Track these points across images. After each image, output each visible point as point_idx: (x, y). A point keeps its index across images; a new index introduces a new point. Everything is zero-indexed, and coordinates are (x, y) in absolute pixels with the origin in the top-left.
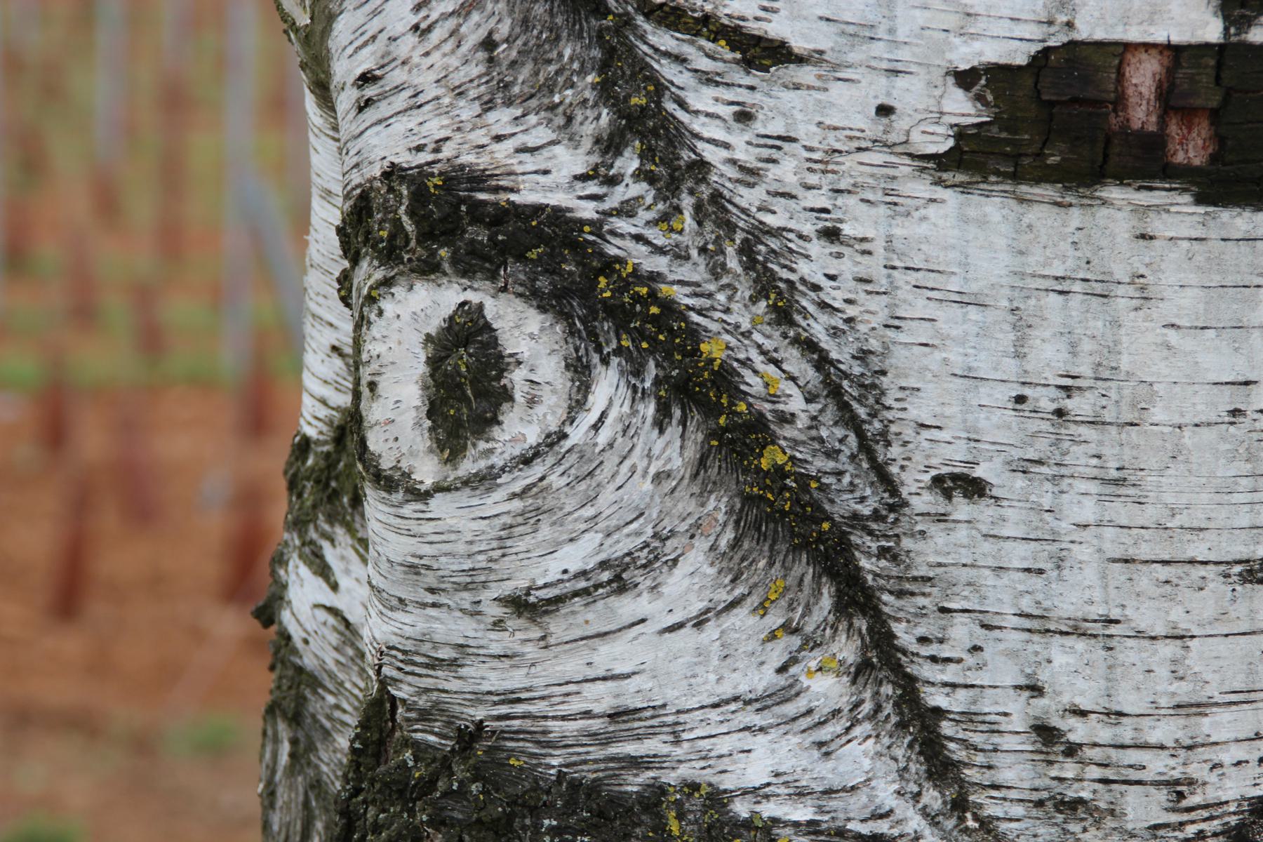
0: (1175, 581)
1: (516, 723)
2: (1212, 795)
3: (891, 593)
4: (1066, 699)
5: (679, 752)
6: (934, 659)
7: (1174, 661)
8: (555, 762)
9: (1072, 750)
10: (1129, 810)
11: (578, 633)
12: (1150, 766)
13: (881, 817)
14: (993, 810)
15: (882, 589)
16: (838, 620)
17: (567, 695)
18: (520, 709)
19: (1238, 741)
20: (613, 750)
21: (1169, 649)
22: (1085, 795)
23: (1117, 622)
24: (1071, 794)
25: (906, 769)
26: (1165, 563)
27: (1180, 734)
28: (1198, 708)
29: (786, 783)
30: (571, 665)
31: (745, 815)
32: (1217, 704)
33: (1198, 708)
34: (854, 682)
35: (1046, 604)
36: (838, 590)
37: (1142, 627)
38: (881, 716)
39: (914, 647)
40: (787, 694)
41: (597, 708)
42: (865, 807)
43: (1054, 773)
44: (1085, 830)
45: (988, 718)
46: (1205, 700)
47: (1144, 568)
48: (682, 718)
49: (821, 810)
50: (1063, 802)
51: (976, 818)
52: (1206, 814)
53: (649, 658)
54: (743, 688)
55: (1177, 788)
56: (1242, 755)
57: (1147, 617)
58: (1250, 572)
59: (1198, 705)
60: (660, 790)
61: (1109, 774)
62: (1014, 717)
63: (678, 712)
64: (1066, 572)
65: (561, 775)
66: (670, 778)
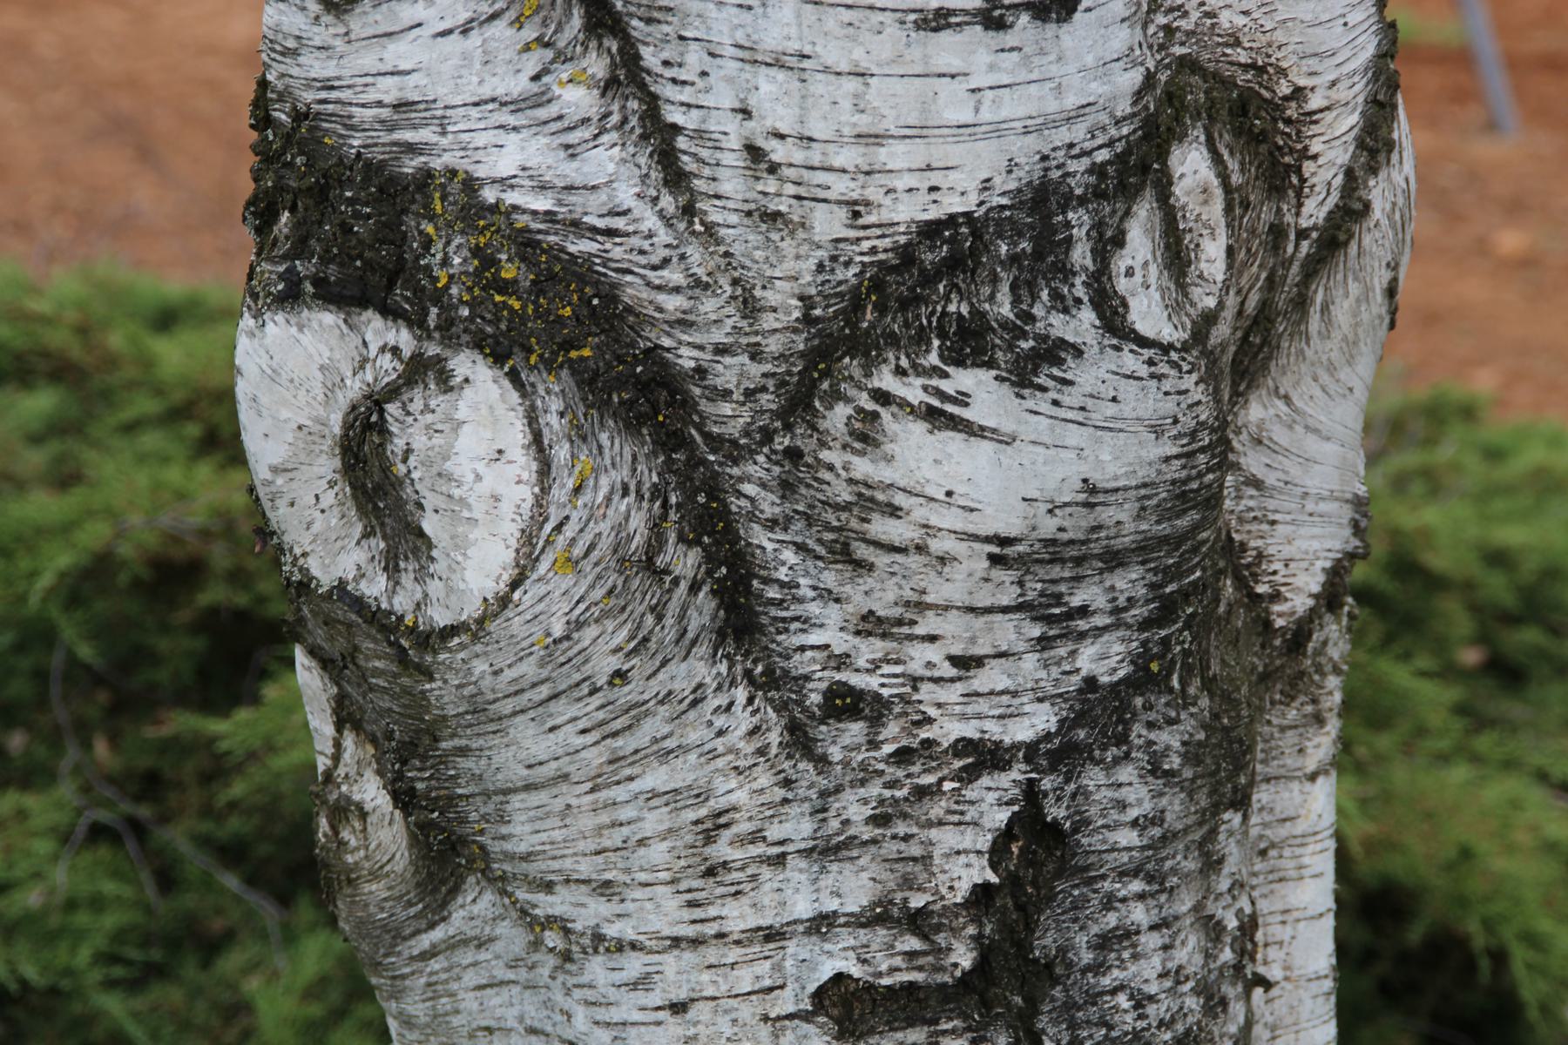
0: (857, 24)
1: (330, 107)
2: (886, 216)
3: (640, 19)
4: (769, 123)
5: (444, 142)
6: (674, 81)
7: (856, 96)
8: (356, 143)
9: (773, 169)
10: (816, 224)
11: (370, 31)
12: (834, 187)
13: (618, 214)
14: (715, 217)
15: (631, 15)
16: (588, 38)
17: (366, 85)
18: (334, 95)
19: (910, 170)
20: (399, 136)
21: (852, 85)
22: (783, 208)
23: (809, 57)
24: (772, 207)
25: (647, 175)
26: (849, 7)
27: (859, 161)
28: (874, 139)
29: (531, 177)
30: (367, 60)
31: (492, 201)
32: (892, 137)
33: (874, 139)
34: (603, 95)
35: (755, 37)
36: (587, 12)
37: (829, 63)
38: (627, 127)
39: (659, 69)
40: (541, 99)
41: (387, 99)
42: (604, 204)
43: (760, 188)
44: (782, 239)
45: (713, 136)
46: (882, 132)
47: (831, 10)
48: (449, 112)
49: (560, 203)
50: (765, 214)
51: (702, 223)
52: (879, 232)
53: (425, 58)
54: (500, 91)
55: (855, 209)
56: (914, 184)
57: (832, 54)
58: (925, 20)
59: (877, 136)
60: (427, 174)
61: (802, 191)
62: (732, 136)
63: (446, 107)
64: (769, 9)
65: (359, 154)
66: (437, 164)
